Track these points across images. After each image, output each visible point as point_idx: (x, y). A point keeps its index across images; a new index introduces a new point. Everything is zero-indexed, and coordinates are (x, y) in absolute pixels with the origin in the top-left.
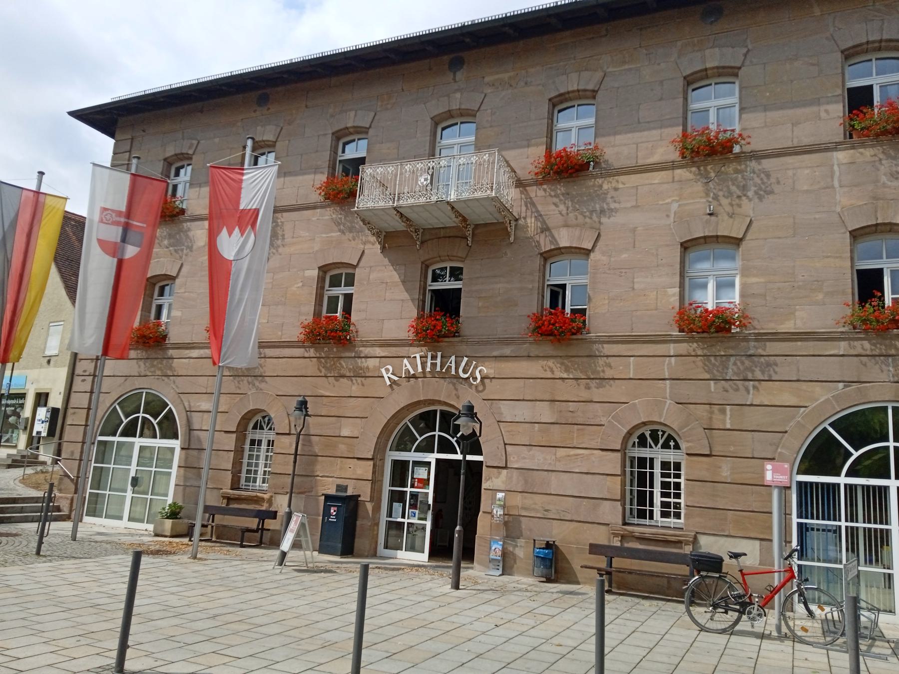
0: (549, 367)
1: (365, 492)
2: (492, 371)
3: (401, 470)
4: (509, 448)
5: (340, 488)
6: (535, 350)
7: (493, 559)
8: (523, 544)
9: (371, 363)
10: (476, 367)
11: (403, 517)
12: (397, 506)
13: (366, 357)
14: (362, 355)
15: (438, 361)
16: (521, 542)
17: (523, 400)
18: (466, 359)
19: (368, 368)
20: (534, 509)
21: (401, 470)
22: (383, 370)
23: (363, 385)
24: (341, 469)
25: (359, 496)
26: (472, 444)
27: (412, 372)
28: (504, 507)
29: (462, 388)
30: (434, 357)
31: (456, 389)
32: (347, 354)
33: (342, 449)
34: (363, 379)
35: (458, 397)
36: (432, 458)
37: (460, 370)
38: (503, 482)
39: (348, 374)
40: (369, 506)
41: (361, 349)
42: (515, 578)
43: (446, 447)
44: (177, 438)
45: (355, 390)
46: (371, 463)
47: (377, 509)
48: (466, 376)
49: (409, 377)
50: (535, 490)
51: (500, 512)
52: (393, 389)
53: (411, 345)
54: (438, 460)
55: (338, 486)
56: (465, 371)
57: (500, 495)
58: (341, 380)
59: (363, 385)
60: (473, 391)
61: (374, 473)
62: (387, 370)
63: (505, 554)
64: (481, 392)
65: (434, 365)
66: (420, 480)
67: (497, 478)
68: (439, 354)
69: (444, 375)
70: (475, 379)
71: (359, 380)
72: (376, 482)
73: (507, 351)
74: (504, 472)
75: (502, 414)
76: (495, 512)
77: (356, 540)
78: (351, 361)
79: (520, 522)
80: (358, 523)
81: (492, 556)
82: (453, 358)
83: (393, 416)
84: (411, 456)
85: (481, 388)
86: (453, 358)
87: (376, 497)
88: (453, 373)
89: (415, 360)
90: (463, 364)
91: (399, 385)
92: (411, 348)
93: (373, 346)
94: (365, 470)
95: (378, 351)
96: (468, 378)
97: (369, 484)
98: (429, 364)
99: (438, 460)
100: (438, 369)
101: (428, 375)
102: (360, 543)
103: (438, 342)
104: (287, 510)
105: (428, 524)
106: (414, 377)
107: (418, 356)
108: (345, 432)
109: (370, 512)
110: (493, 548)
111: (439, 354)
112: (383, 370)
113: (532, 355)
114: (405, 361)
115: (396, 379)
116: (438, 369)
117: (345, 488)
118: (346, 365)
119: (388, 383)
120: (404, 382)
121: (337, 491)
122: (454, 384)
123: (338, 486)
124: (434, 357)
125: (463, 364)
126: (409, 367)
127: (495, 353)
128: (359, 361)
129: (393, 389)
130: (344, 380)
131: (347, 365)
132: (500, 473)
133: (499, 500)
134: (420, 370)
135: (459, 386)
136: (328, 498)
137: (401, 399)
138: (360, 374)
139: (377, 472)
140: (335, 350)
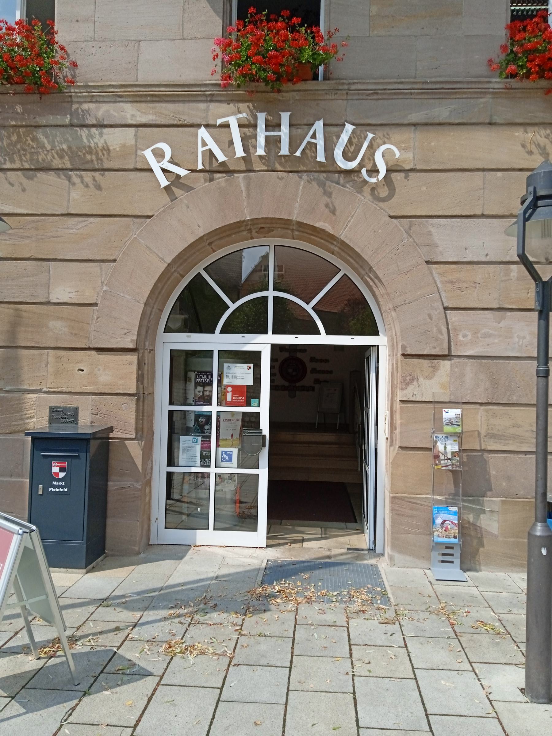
0: (538, 145)
1: (122, 419)
2: (410, 155)
3: (189, 369)
4: (453, 316)
5: (63, 415)
6: (504, 110)
7: (438, 544)
8: (496, 508)
9: (115, 139)
10: (372, 148)
11: (205, 460)
12: (190, 446)
13: (101, 126)
14: (91, 121)
15: (284, 132)
16: (492, 502)
17: (483, 216)
18: (349, 128)
19: (106, 149)
20: (514, 437)
21: (189, 369)
22: (148, 154)
23: (99, 188)
24: (57, 373)
25: (111, 429)
26: (352, 313)
27: (221, 157)
28: (459, 437)
29: (342, 194)
30: (273, 125)
31: (329, 195)
32: (51, 119)
33: (58, 329)
34: (97, 174)
35: (333, 212)
36: (263, 343)
37: (338, 152)
38: (443, 386)
39: (57, 163)
40: (135, 449)
41: (85, 106)
42: (484, 574)
43: (289, 320)
44: (21, 617)
45: (77, 195)
46: (133, 358)
47: (148, 453)
48: (353, 165)
49: (214, 169)
50: (514, 399)
51: (453, 447)
52: (173, 198)
53: (212, 99)
54: (275, 348)
55: (52, 410)
56: (348, 156)
57: (451, 413)
58: (41, 175)
59: (99, 188)
60: (366, 197)
61: (140, 379)
62: (159, 155)
63: (464, 528)
64: (383, 200)
65: (272, 143)
66: (237, 389)
67: (428, 378)
68: (285, 117)
69: (300, 165)
70: (374, 171)
71: (88, 177)
72: (143, 397)
73: (442, 111)
74: (446, 364)
75: (435, 246)
76: (440, 447)
77: (109, 522)
78: (68, 134)
79: (486, 462)
80: (112, 485)
81: (438, 537)
82: (319, 126)
83: (179, 256)
84: (216, 341)
85: (384, 192)
86: (319, 126)
87: (144, 431)
88: (321, 158)
89: (228, 131)
90: (344, 138)
91: (188, 189)
92: (212, 106)
93: (117, 98)
94: (120, 373)
95: (131, 112)
96: (356, 171)
97: (131, 403)
98: (261, 140)
99: (275, 348)
100: (285, 150)
101: (258, 166)
102: (116, 528)
103: (279, 91)
104: (297, 617)
105: (263, 474)
106: (225, 169)
107: (233, 122)
108: (62, 293)
109: (140, 468)
110: (439, 521)
111: (285, 117)
112: (148, 154)
113: (496, 119)
114: (203, 132)
115: (182, 172)
116: (285, 150)
117: (73, 415)
118: (51, 143)
119: (164, 182)
120: (200, 181)
121: (52, 420)
122: (322, 184)
123: (52, 410)
124: (273, 125)
125: (344, 138)
126: (213, 146)
127: (414, 117)
128: (84, 133)
129: (173, 198)
130: (51, 177)
131: (52, 143)
132: (435, 369)
133: (451, 423)
134: (240, 152)
135: (332, 187)
136: (40, 441)
137: (194, 219)
138: (87, 164)
139: (144, 374)
140: (19, 108)
